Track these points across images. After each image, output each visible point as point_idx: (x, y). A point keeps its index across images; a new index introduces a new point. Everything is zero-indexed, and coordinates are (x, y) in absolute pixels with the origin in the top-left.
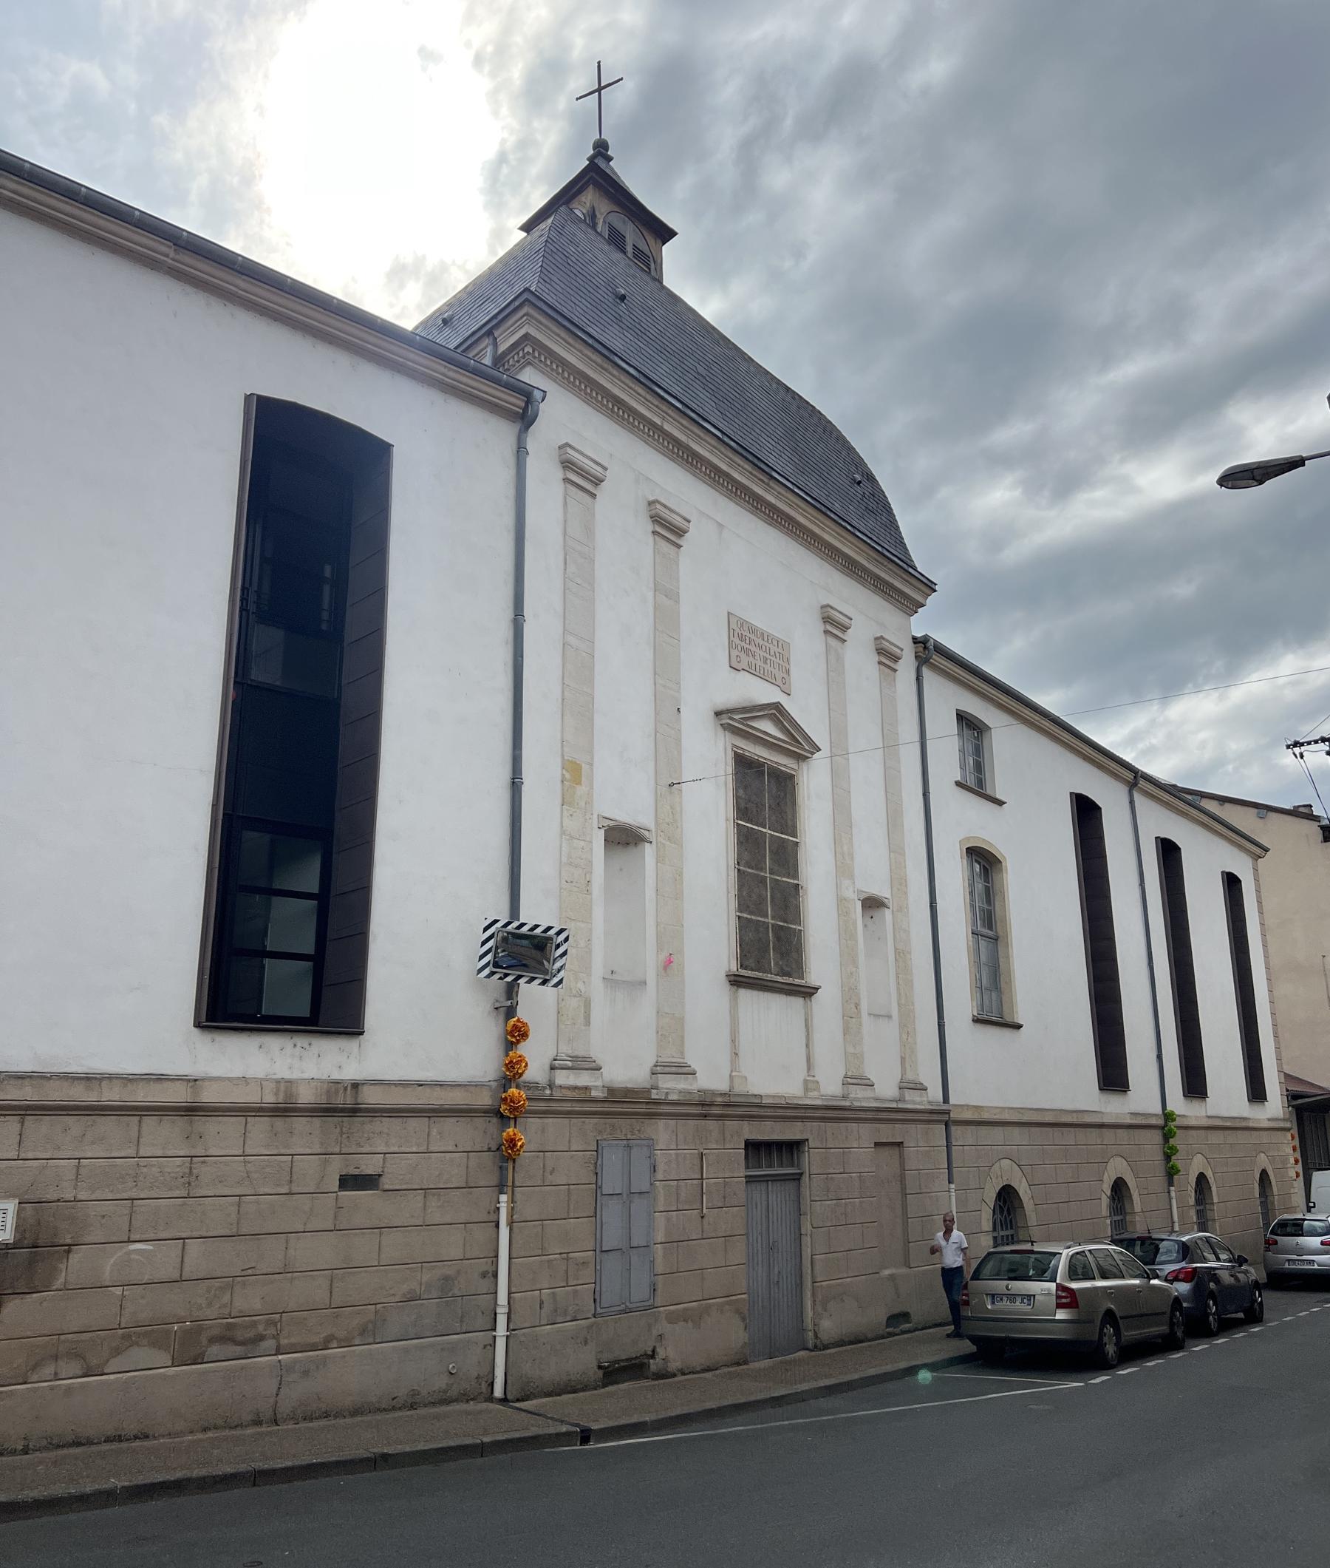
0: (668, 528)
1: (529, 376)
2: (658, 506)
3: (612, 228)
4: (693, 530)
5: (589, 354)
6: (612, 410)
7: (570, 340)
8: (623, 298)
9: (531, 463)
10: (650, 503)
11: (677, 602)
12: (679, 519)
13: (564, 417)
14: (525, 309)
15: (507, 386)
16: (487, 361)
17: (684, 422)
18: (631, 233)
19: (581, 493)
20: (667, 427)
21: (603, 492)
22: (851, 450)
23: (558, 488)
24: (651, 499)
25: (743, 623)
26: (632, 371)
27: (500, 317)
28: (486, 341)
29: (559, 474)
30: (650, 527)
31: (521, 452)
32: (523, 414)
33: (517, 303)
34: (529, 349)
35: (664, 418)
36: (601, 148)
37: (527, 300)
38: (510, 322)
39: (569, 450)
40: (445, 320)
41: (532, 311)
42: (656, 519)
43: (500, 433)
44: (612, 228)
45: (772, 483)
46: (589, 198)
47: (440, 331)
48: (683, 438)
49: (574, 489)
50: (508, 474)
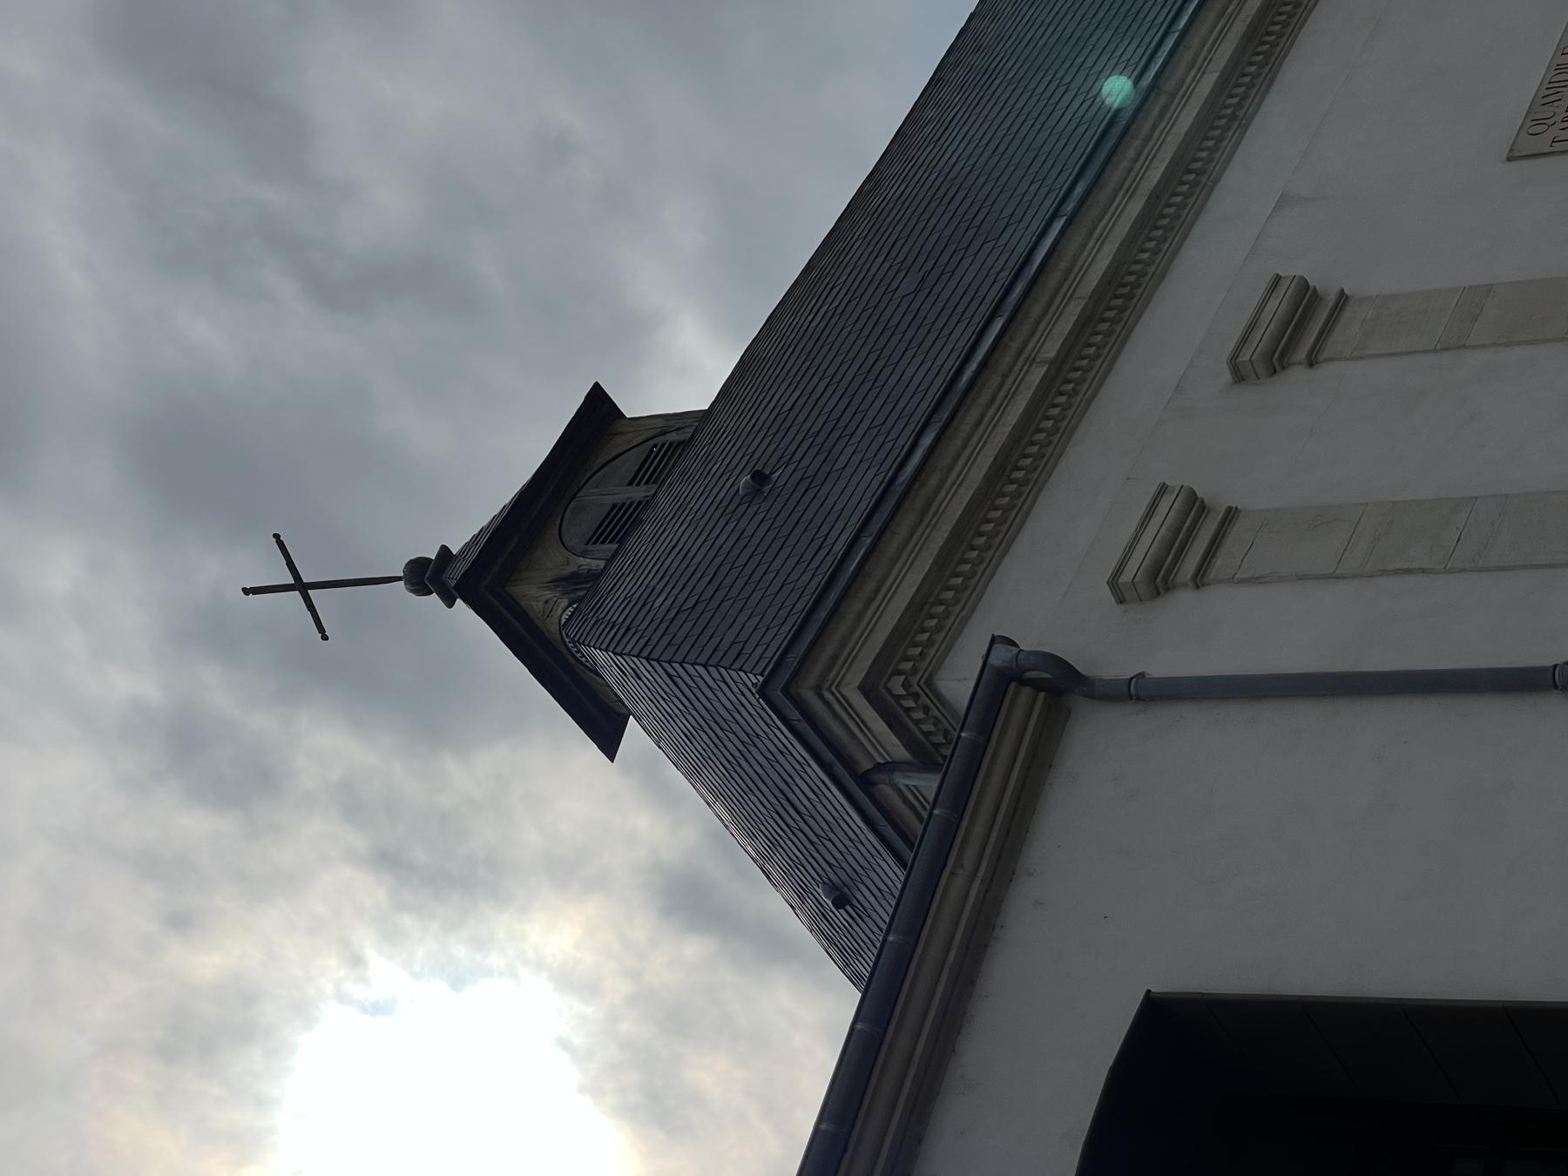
0: (1295, 330)
1: (958, 681)
2: (1245, 356)
3: (597, 537)
4: (1290, 269)
5: (896, 541)
6: (1023, 483)
7: (870, 586)
8: (760, 478)
9: (1165, 664)
10: (1239, 376)
11: (1488, 289)
12: (1273, 304)
13: (1051, 592)
14: (809, 695)
15: (986, 727)
16: (927, 784)
17: (1037, 309)
18: (604, 493)
19: (1228, 543)
20: (1051, 350)
21: (1218, 490)
22: (972, 16)
23: (1218, 600)
24: (1227, 376)
25: (1535, 120)
26: (927, 440)
27: (828, 756)
28: (885, 790)
29: (1184, 601)
30: (1297, 376)
31: (1141, 692)
32: (1044, 693)
33: (795, 715)
34: (898, 683)
35: (1032, 360)
36: (427, 576)
37: (786, 691)
38: (838, 730)
39: (1127, 577)
40: (831, 901)
41: (811, 680)
42: (1277, 360)
43: (1099, 751)
44: (597, 537)
45: (1169, 86)
46: (536, 595)
47: (862, 913)
48: (1073, 312)
49: (1219, 561)
50: (1194, 734)
